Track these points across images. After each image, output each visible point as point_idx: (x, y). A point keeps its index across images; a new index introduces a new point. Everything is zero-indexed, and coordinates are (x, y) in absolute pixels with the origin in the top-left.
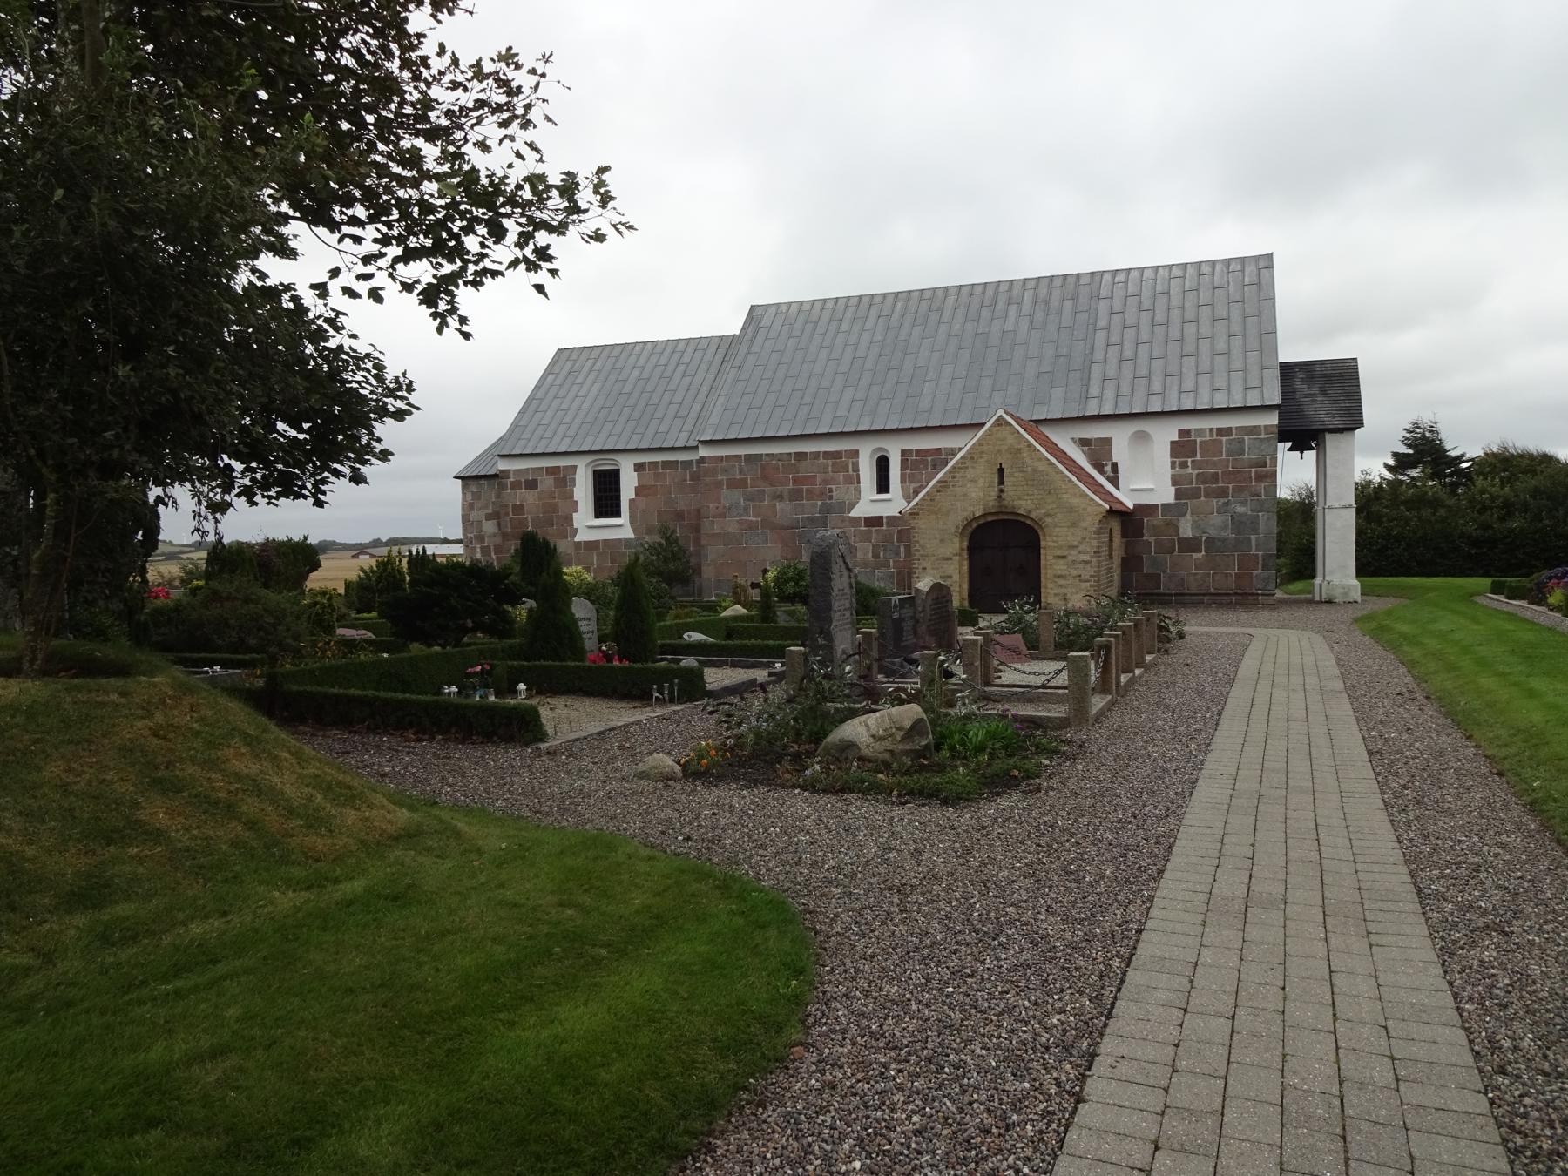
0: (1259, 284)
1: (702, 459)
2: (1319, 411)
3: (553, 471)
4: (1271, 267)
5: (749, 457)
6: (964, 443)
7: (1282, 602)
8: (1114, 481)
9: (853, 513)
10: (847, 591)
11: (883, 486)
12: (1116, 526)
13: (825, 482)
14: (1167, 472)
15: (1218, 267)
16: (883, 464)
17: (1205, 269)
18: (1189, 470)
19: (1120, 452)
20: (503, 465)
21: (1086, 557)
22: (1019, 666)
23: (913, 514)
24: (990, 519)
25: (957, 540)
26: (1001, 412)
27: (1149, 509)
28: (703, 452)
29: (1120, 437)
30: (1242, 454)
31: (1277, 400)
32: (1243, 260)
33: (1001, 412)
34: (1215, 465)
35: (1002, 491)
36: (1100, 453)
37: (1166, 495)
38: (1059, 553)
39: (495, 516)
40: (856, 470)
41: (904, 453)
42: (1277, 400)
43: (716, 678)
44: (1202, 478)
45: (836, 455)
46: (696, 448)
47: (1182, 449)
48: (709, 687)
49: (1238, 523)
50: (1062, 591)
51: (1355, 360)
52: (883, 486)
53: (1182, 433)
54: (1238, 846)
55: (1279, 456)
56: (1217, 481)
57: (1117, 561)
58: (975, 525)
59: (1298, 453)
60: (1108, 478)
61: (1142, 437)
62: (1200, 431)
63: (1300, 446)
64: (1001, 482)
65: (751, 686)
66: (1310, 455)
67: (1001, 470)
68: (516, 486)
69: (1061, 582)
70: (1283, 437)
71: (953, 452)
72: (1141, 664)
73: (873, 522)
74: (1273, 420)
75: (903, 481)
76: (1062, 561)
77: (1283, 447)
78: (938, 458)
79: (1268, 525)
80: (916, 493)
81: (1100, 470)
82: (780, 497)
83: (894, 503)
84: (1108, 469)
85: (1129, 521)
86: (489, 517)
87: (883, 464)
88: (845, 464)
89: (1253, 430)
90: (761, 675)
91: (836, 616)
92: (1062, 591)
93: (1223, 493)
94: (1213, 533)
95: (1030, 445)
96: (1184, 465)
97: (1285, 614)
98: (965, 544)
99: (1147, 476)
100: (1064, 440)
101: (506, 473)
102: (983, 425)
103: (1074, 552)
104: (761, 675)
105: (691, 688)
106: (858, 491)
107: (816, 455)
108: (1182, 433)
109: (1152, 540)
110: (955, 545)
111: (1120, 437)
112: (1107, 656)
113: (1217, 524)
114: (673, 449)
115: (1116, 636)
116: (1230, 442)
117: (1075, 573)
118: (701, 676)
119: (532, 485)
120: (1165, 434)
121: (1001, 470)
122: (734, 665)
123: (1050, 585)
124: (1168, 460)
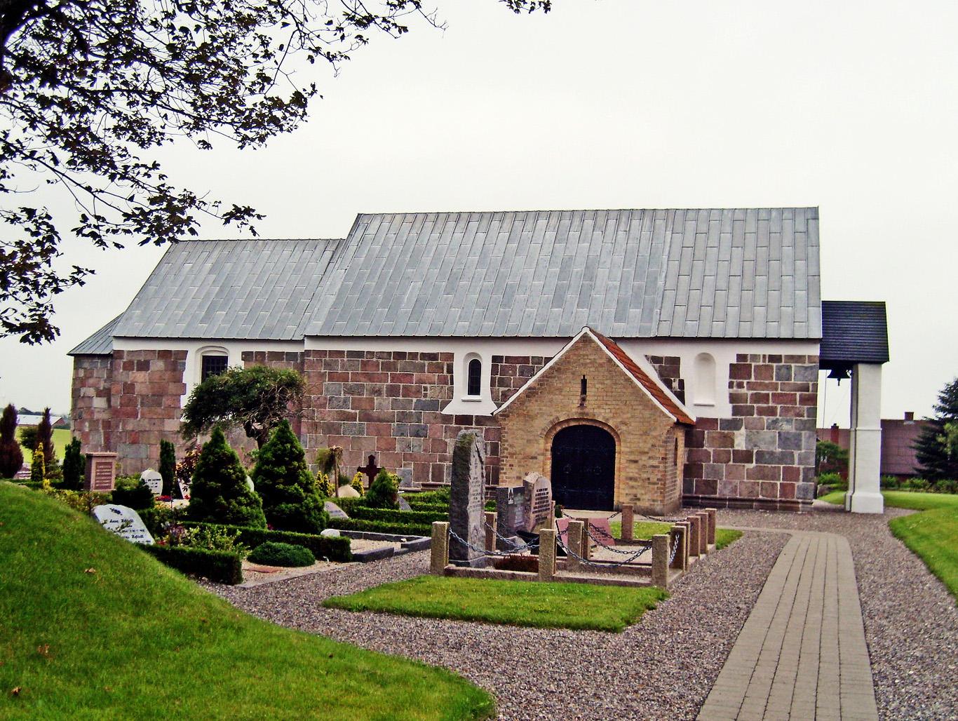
0: (807, 232)
1: (307, 353)
2: (856, 337)
3: (164, 354)
4: (816, 218)
5: (351, 354)
6: (556, 353)
7: (822, 511)
8: (681, 396)
9: (446, 411)
10: (480, 479)
11: (474, 388)
12: (680, 436)
13: (420, 381)
14: (725, 392)
15: (774, 214)
16: (475, 368)
17: (763, 215)
18: (744, 391)
19: (688, 370)
20: (118, 346)
21: (655, 463)
22: (612, 547)
23: (505, 415)
24: (572, 424)
25: (542, 441)
26: (586, 330)
27: (711, 423)
28: (309, 346)
29: (687, 356)
30: (789, 379)
31: (818, 334)
32: (794, 211)
33: (586, 330)
34: (767, 387)
35: (584, 399)
36: (669, 369)
37: (724, 411)
38: (632, 457)
39: (106, 394)
40: (450, 370)
41: (496, 359)
42: (818, 334)
43: (358, 546)
44: (758, 398)
45: (433, 357)
46: (302, 342)
47: (739, 370)
48: (353, 552)
49: (784, 439)
50: (634, 491)
51: (878, 310)
52: (474, 388)
53: (741, 357)
54: (774, 644)
55: (820, 382)
56: (767, 402)
57: (680, 467)
58: (559, 429)
59: (836, 380)
60: (676, 393)
61: (705, 359)
62: (755, 357)
63: (838, 373)
64: (584, 391)
65: (390, 553)
66: (846, 382)
67: (584, 382)
68: (128, 366)
69: (632, 483)
70: (824, 364)
71: (540, 361)
72: (704, 551)
73: (464, 420)
74: (815, 351)
75: (493, 384)
76: (633, 465)
77: (824, 374)
78: (528, 366)
79: (808, 446)
80: (505, 396)
81: (669, 384)
82: (378, 392)
83: (485, 405)
84: (675, 385)
85: (692, 431)
86: (99, 394)
87: (475, 368)
88: (442, 365)
89: (799, 359)
90: (397, 546)
91: (471, 498)
92: (634, 491)
93: (772, 412)
94: (763, 448)
95: (610, 360)
96: (740, 386)
97: (816, 520)
98: (549, 445)
99: (708, 393)
100: (637, 355)
101: (119, 354)
102: (571, 338)
103: (644, 458)
104: (397, 546)
105: (338, 551)
106: (451, 391)
107: (414, 355)
108: (741, 357)
109: (711, 450)
110: (544, 446)
111: (687, 356)
112: (681, 540)
113: (769, 441)
114: (280, 341)
115: (686, 525)
116: (779, 368)
117: (645, 476)
118: (348, 543)
119: (144, 366)
120: (726, 357)
121: (584, 382)
122: (366, 537)
123: (622, 486)
124: (727, 380)
